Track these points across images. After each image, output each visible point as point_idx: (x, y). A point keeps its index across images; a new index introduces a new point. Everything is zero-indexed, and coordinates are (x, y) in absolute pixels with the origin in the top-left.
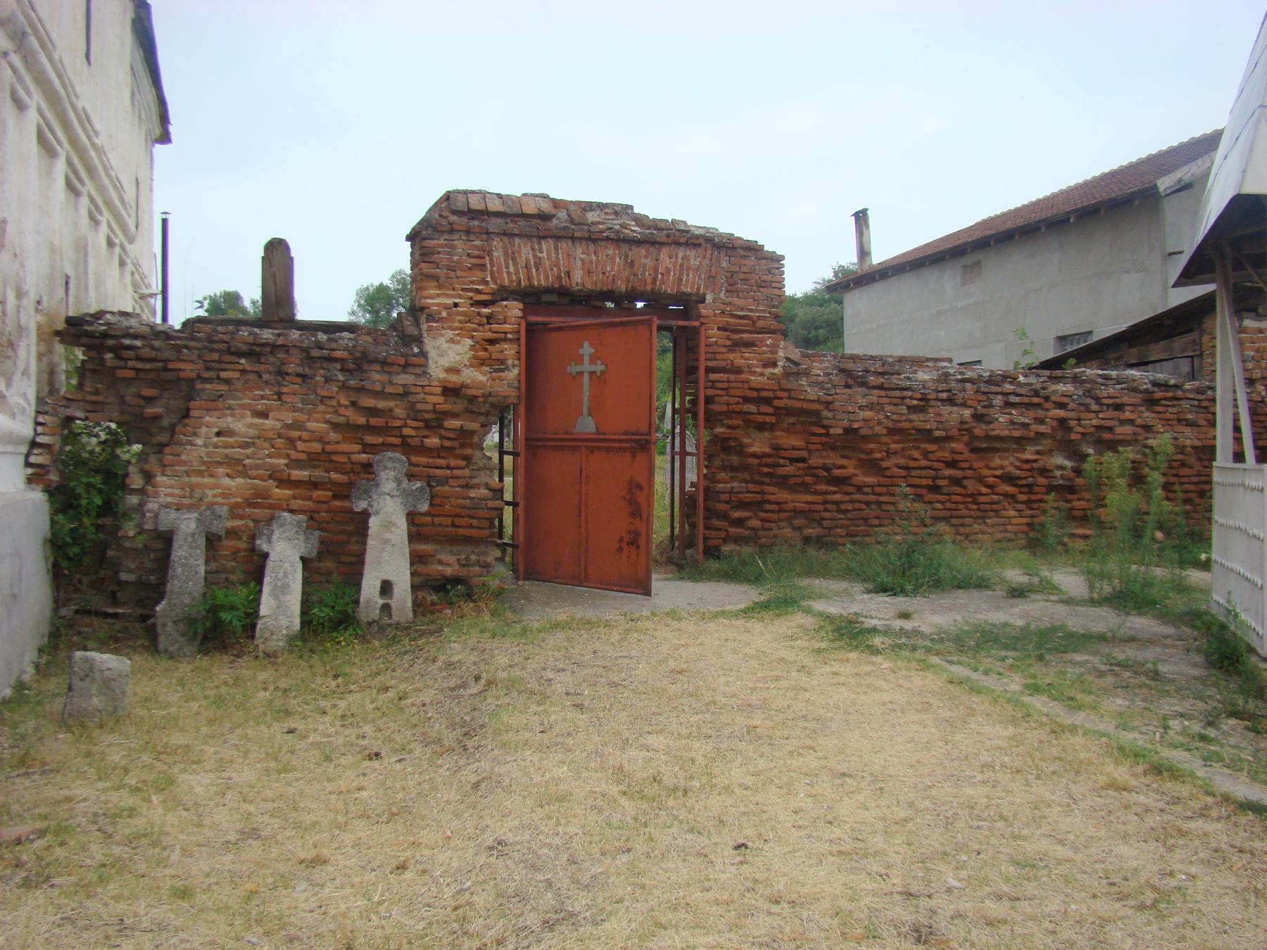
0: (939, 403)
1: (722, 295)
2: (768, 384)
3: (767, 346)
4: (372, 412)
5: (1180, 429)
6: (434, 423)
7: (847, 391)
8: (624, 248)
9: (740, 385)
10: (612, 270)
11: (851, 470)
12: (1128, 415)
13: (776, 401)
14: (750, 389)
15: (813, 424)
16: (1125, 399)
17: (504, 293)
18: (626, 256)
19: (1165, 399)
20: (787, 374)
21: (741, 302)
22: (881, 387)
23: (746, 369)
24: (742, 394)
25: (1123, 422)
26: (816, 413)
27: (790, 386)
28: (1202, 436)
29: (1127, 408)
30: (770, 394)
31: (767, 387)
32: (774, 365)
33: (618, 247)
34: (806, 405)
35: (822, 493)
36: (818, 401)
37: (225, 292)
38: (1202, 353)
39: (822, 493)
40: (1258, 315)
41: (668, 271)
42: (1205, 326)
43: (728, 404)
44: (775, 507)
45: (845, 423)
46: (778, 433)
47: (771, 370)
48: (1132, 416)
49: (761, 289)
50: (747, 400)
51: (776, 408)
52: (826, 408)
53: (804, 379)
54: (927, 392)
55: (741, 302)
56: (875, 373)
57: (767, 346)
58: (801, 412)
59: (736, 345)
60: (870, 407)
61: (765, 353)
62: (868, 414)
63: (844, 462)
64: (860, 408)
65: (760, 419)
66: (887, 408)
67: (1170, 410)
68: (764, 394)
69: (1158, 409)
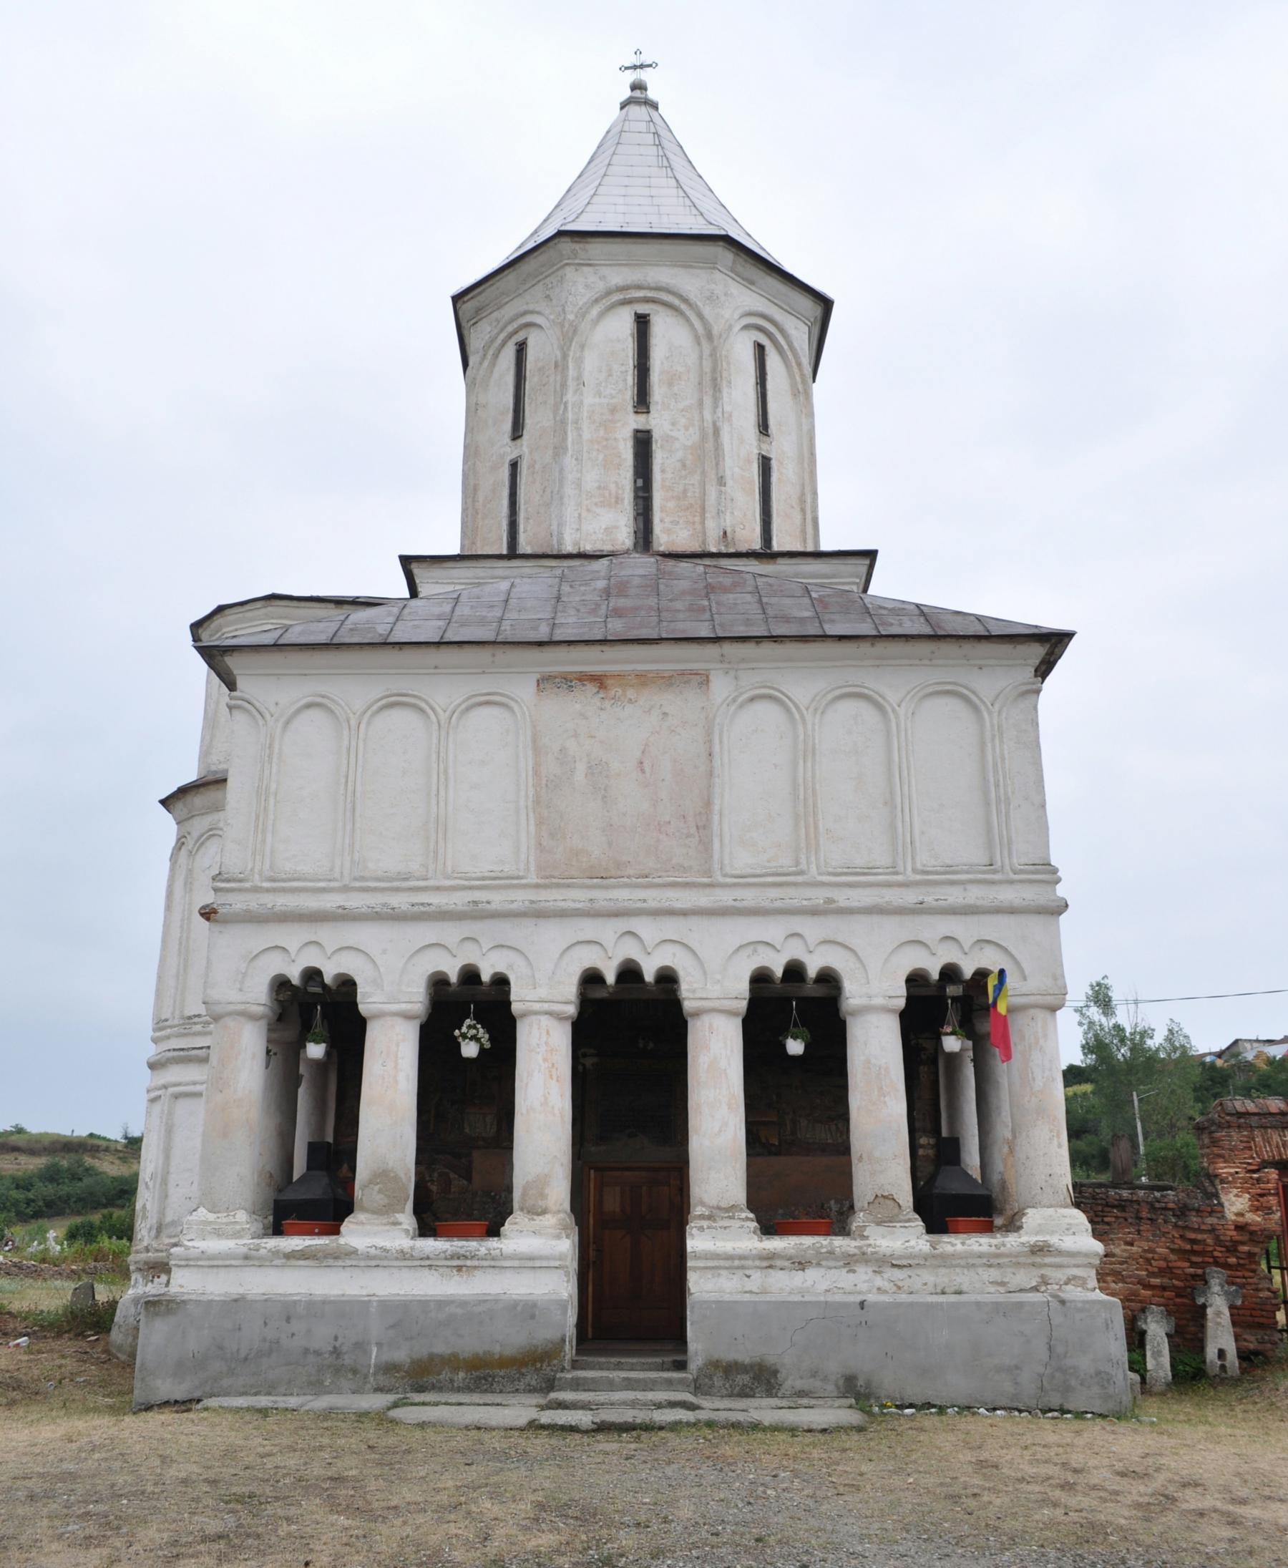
4: (1193, 1241)
6: (1232, 1248)
17: (1265, 1164)
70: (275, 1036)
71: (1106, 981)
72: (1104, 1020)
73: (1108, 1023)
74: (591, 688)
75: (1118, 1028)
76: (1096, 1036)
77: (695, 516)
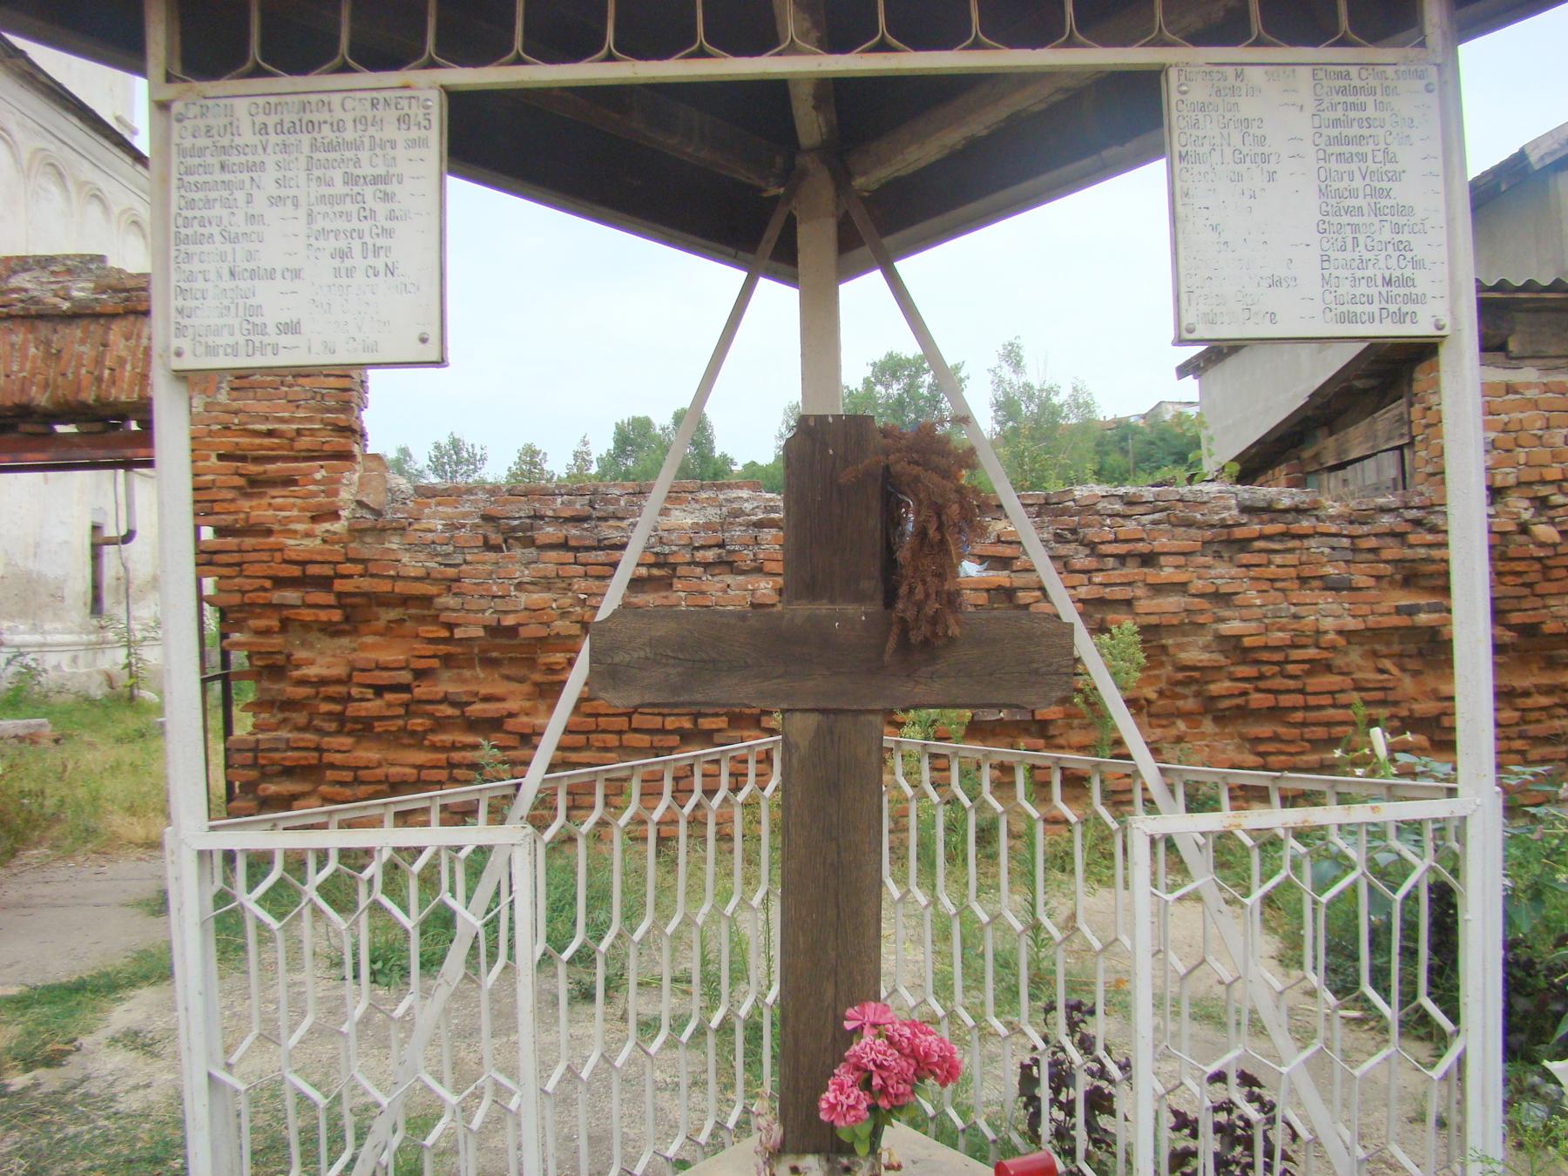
0: (699, 570)
1: (223, 397)
2: (321, 553)
3: (316, 482)
5: (1307, 595)
7: (492, 556)
8: (44, 329)
9: (265, 556)
10: (21, 370)
11: (512, 705)
12: (1167, 573)
13: (337, 582)
14: (285, 561)
15: (422, 620)
16: (1162, 542)
18: (48, 344)
19: (1262, 537)
20: (356, 532)
21: (262, 407)
22: (564, 545)
23: (276, 527)
24: (271, 573)
25: (1158, 589)
26: (427, 600)
27: (366, 553)
28: (1365, 609)
29: (1163, 560)
30: (327, 570)
31: (319, 558)
32: (335, 516)
33: (33, 330)
34: (400, 587)
35: (443, 748)
36: (427, 577)
37: (634, 418)
38: (1413, 438)
39: (443, 748)
40: (1509, 357)
41: (122, 362)
42: (1416, 387)
43: (243, 593)
44: (347, 776)
45: (489, 617)
46: (369, 639)
47: (327, 526)
48: (1181, 577)
49: (301, 381)
50: (280, 582)
51: (340, 595)
52: (449, 589)
53: (396, 539)
54: (666, 550)
55: (262, 407)
56: (557, 519)
57: (316, 482)
58: (405, 600)
59: (255, 485)
60: (545, 583)
61: (314, 495)
62: (538, 598)
63: (500, 688)
64: (520, 586)
65: (307, 615)
66: (579, 584)
67: (1278, 559)
68: (313, 570)
69: (1245, 558)
71: (1018, 341)
72: (1014, 378)
73: (1018, 381)
74: (1326, 763)
75: (1027, 386)
76: (1006, 394)
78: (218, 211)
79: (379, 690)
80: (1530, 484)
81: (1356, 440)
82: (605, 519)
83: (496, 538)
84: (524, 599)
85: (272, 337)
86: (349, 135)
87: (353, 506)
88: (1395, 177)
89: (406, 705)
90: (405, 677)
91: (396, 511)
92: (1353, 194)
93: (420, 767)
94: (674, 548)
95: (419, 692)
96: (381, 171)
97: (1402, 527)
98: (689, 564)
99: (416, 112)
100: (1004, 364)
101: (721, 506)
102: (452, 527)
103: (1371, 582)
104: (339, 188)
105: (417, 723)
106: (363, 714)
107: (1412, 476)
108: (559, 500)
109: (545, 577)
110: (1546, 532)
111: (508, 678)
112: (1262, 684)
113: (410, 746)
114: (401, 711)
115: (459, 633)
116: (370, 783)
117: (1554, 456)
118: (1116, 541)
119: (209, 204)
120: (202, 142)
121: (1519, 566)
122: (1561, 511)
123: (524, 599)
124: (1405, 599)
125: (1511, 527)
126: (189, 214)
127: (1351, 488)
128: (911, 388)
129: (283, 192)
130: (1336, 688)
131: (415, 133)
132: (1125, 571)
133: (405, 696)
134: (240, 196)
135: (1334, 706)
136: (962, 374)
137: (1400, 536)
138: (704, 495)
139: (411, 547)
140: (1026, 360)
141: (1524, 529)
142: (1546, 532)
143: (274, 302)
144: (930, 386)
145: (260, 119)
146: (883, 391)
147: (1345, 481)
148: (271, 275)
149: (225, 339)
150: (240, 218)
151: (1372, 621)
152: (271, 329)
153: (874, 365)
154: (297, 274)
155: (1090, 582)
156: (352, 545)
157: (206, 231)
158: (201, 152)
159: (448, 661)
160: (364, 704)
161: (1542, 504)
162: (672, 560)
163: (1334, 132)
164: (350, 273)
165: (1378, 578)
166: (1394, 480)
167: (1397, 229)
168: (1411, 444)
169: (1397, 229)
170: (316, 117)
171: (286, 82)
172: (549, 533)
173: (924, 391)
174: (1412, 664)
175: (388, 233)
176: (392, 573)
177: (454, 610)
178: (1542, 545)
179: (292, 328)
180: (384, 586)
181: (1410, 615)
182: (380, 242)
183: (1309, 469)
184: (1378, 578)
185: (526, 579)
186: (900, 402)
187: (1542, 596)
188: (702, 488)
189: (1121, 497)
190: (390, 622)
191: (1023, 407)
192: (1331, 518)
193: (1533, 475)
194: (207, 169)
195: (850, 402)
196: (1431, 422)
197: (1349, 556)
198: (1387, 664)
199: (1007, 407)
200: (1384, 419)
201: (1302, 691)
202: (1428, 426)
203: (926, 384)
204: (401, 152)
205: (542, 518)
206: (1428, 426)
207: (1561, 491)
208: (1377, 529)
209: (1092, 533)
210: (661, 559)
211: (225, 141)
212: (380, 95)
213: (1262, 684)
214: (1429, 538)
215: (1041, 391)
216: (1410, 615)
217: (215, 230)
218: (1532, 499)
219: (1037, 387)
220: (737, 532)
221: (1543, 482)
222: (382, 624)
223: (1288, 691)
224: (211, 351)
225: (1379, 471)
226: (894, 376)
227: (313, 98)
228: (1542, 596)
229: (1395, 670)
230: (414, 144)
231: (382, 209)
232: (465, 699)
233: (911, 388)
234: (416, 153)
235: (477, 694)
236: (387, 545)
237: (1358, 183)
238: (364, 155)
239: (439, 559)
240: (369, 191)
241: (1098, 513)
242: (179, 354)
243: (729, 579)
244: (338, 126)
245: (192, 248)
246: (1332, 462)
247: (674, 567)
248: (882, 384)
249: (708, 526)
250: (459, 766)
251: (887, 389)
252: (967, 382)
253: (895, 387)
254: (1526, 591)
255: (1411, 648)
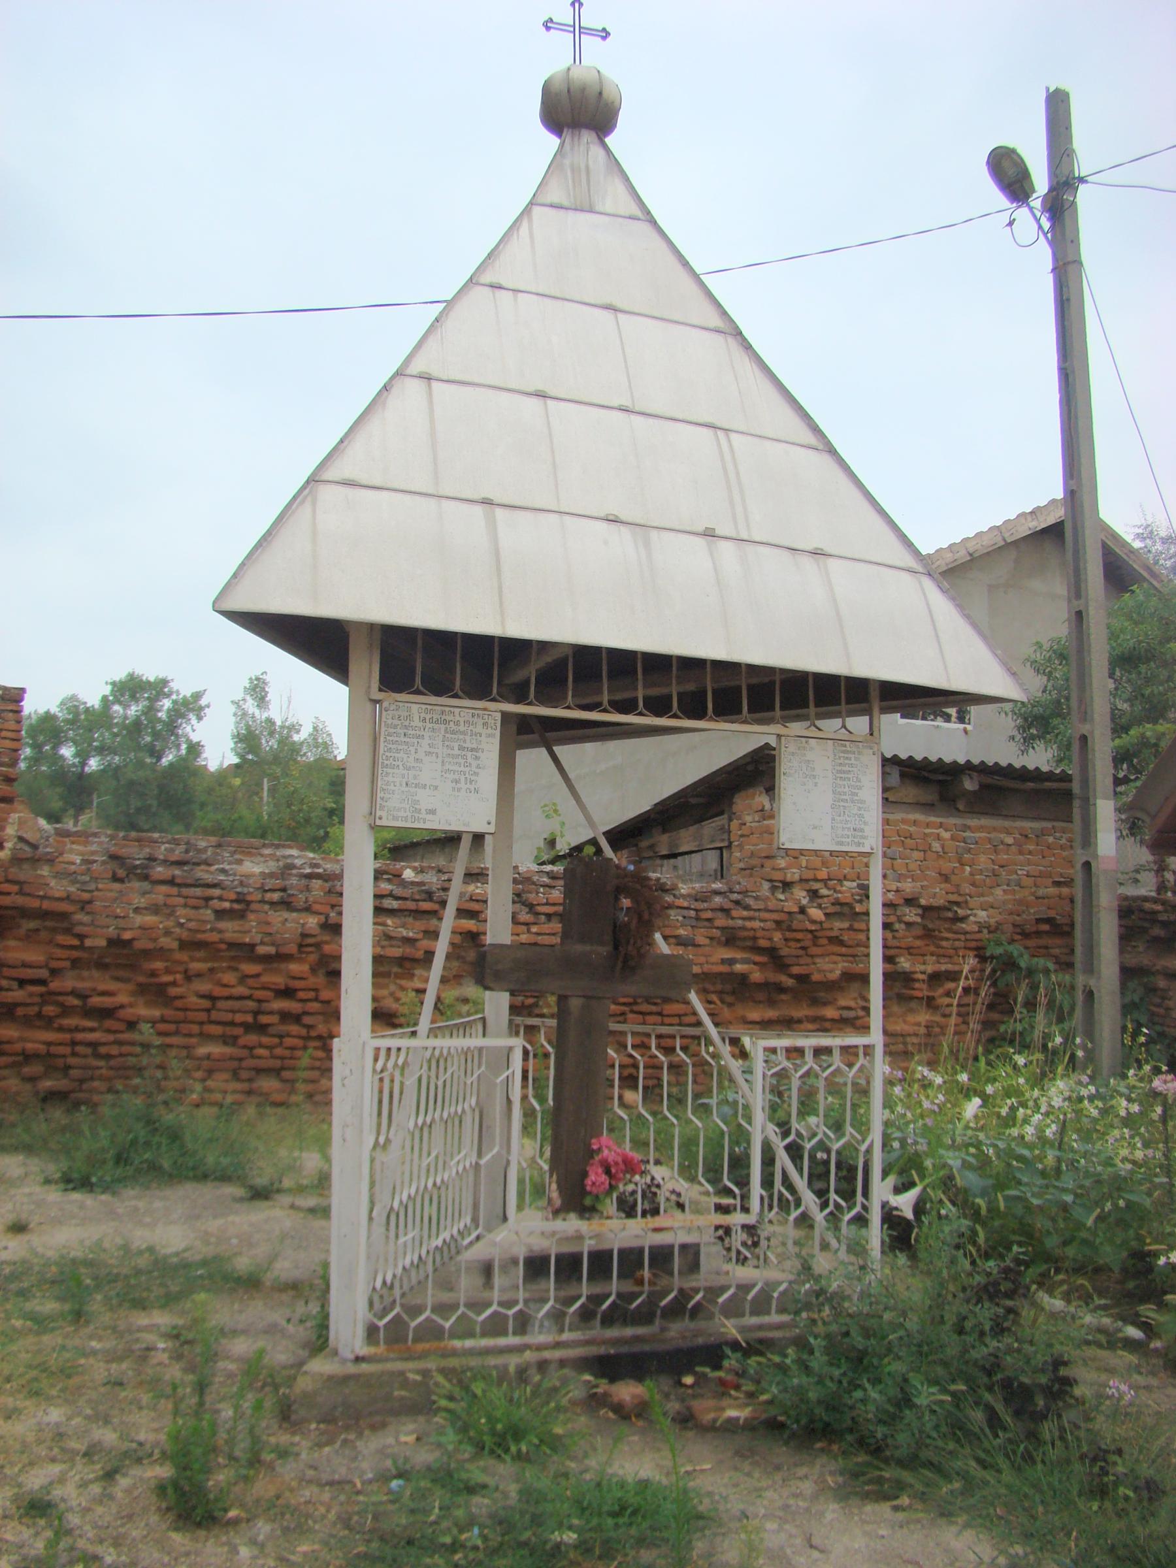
0: (267, 907)
7: (117, 886)
11: (122, 999)
20: (17, 860)
22: (171, 882)
26: (63, 916)
27: (22, 877)
34: (46, 905)
35: (70, 1030)
36: (68, 898)
38: (731, 843)
42: (735, 808)
46: (12, 943)
52: (82, 909)
54: (245, 890)
58: (44, 915)
62: (150, 919)
63: (112, 986)
64: (137, 910)
70: (778, 678)
71: (264, 677)
72: (257, 712)
75: (270, 721)
76: (248, 727)
77: (310, 1431)
78: (401, 755)
79: (22, 983)
80: (807, 881)
81: (686, 839)
82: (198, 864)
83: (121, 873)
84: (139, 920)
85: (423, 815)
86: (462, 728)
87: (15, 840)
88: (860, 788)
89: (42, 995)
90: (43, 973)
91: (46, 846)
92: (845, 794)
93: (49, 1044)
94: (251, 890)
95: (55, 985)
96: (474, 746)
97: (728, 905)
98: (260, 902)
99: (491, 721)
100: (248, 698)
101: (278, 860)
102: (86, 862)
103: (707, 941)
104: (456, 752)
105: (49, 1010)
106: (10, 1000)
107: (728, 870)
108: (163, 848)
109: (156, 905)
110: (816, 913)
111: (117, 979)
112: (635, 1008)
113: (39, 1027)
114: (37, 999)
115: (88, 943)
116: (11, 1055)
117: (823, 863)
118: (547, 904)
119: (398, 751)
120: (396, 722)
121: (799, 936)
122: (825, 899)
123: (139, 920)
124: (727, 954)
125: (796, 909)
126: (388, 754)
127: (681, 872)
128: (151, 710)
129: (432, 750)
130: (682, 1012)
131: (490, 731)
132: (551, 925)
133: (42, 989)
134: (412, 749)
135: (680, 1025)
136: (203, 702)
137: (725, 911)
138: (267, 851)
139: (57, 875)
140: (272, 696)
141: (802, 910)
142: (816, 913)
143: (426, 799)
144: (169, 710)
145: (423, 715)
146: (121, 711)
147: (675, 868)
148: (424, 786)
149: (402, 814)
150: (411, 759)
151: (706, 968)
152: (423, 811)
153: (114, 684)
154: (436, 788)
155: (529, 931)
156: (12, 870)
157: (396, 763)
158: (395, 727)
159: (75, 963)
160: (11, 993)
161: (814, 894)
162: (249, 898)
163: (839, 768)
164: (459, 790)
165: (711, 939)
166: (716, 871)
167: (860, 809)
168: (729, 847)
169: (860, 809)
170: (448, 718)
171: (433, 699)
172: (159, 871)
173: (162, 715)
174: (729, 999)
175: (476, 774)
176: (41, 893)
177: (85, 925)
178: (813, 922)
179: (432, 812)
180: (35, 904)
181: (730, 965)
182: (473, 778)
183: (645, 855)
184: (711, 939)
185: (142, 905)
186: (137, 723)
187: (812, 956)
188: (264, 846)
189: (547, 873)
190: (29, 930)
191: (263, 741)
192: (683, 896)
193: (809, 875)
194: (398, 735)
195: (86, 719)
196: (745, 833)
197: (694, 923)
198: (714, 997)
199: (247, 739)
200: (710, 827)
201: (660, 1014)
202: (742, 836)
203: (166, 708)
204: (483, 738)
205: (155, 860)
206: (742, 836)
207: (826, 886)
208: (713, 906)
209: (531, 897)
210: (241, 897)
211: (407, 723)
212: (476, 712)
213: (635, 1008)
214: (745, 913)
215: (282, 727)
216: (730, 965)
217: (400, 763)
218: (808, 891)
219: (279, 723)
220: (294, 881)
221: (816, 880)
222: (22, 931)
223: (651, 1013)
224: (395, 818)
225: (703, 863)
226: (134, 697)
227: (447, 709)
228: (812, 956)
229: (718, 1002)
230: (489, 736)
231: (474, 763)
232: (88, 993)
233: (151, 710)
234: (490, 740)
235: (94, 990)
236: (39, 872)
237: (847, 789)
238: (468, 738)
239: (78, 886)
240: (469, 754)
241: (534, 883)
242: (380, 818)
243: (286, 915)
244: (457, 723)
245: (389, 770)
246: (665, 852)
247: (248, 903)
248: (120, 703)
249: (272, 875)
250: (81, 1043)
251: (125, 709)
252: (207, 710)
253: (134, 708)
254: (801, 952)
255: (728, 987)
